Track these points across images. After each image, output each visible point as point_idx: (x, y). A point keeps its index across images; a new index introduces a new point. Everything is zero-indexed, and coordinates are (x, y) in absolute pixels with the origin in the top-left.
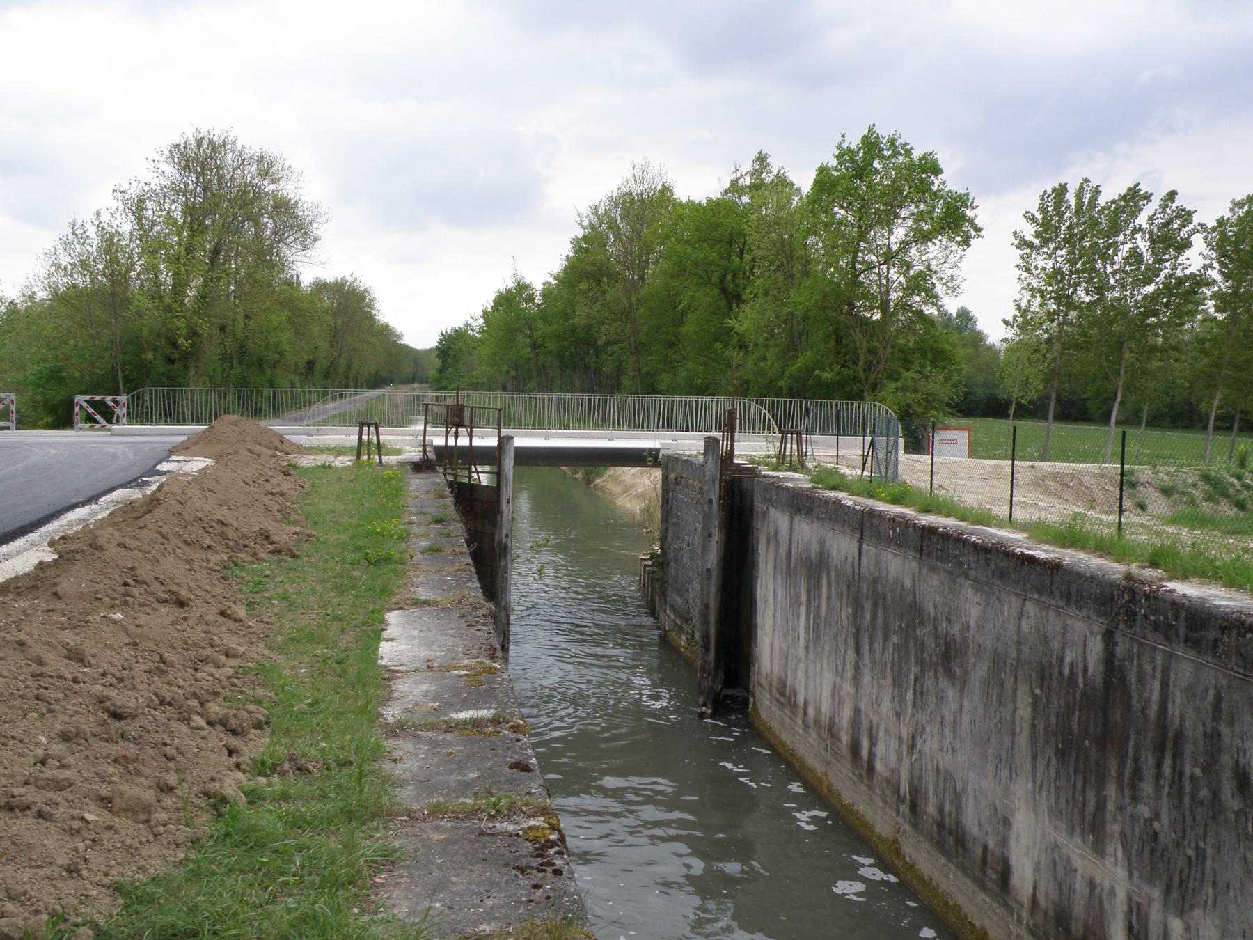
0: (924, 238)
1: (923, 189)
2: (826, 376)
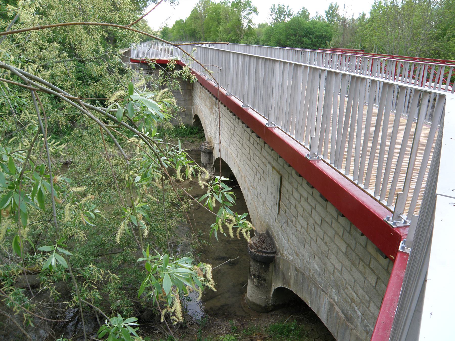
0: (250, 14)
1: (250, 6)
2: (233, 38)
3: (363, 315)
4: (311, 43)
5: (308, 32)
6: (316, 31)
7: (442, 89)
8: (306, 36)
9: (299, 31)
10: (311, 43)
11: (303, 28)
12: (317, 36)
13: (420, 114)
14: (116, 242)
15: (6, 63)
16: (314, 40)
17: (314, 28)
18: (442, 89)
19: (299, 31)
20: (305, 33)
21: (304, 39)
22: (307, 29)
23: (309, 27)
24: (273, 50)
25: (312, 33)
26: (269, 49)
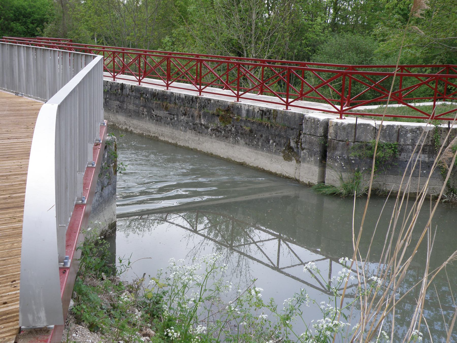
3: (384, 108)
4: (25, 30)
5: (21, 12)
6: (33, 13)
7: (104, 76)
8: (16, 19)
9: (3, 12)
10: (25, 30)
11: (12, 7)
12: (36, 20)
13: (257, 101)
14: (210, 221)
15: (167, 100)
16: (31, 26)
17: (31, 8)
18: (104, 76)
19: (3, 12)
20: (15, 15)
21: (13, 24)
22: (18, 9)
23: (22, 6)
24: (15, 50)
25: (27, 16)
26: (39, 51)
